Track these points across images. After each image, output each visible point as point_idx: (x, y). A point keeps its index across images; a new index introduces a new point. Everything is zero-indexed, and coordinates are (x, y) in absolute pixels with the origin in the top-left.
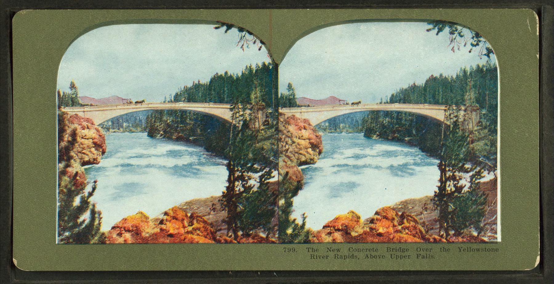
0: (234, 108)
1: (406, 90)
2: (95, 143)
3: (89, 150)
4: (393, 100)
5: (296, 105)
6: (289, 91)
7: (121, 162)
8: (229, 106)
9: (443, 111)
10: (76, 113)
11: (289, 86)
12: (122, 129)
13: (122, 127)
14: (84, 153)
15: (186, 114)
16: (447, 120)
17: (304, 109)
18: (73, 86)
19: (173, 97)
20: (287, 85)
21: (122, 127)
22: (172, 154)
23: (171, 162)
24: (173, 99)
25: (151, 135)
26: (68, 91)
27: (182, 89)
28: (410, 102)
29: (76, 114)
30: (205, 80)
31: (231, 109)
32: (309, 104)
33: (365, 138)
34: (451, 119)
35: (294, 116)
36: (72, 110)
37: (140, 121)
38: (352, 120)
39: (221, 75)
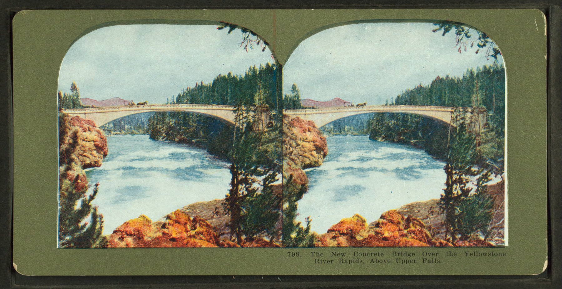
0: (238, 109)
1: (412, 91)
2: (96, 146)
3: (90, 152)
4: (399, 101)
5: (300, 107)
6: (293, 92)
7: (123, 165)
8: (232, 108)
9: (450, 113)
10: (77, 115)
11: (293, 88)
12: (123, 132)
13: (124, 129)
14: (85, 156)
15: (188, 116)
16: (454, 122)
17: (308, 111)
18: (74, 88)
19: (175, 99)
20: (291, 86)
21: (124, 129)
22: (175, 157)
23: (174, 165)
24: (175, 101)
25: (154, 137)
26: (69, 93)
27: (185, 91)
28: (415, 104)
29: (77, 116)
30: (208, 81)
31: (235, 111)
32: (314, 106)
33: (150, 140)
34: (457, 121)
35: (298, 118)
36: (73, 112)
37: (143, 123)
38: (358, 122)
39: (224, 77)
